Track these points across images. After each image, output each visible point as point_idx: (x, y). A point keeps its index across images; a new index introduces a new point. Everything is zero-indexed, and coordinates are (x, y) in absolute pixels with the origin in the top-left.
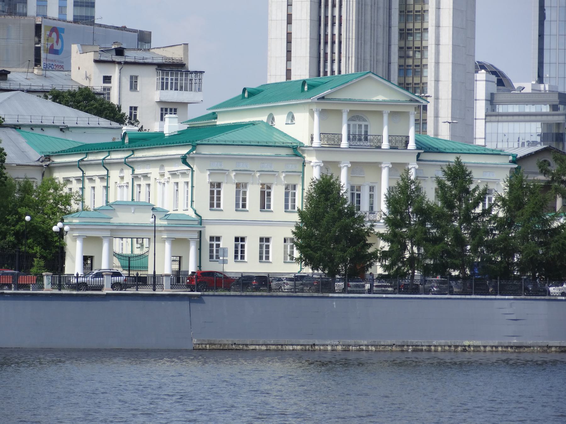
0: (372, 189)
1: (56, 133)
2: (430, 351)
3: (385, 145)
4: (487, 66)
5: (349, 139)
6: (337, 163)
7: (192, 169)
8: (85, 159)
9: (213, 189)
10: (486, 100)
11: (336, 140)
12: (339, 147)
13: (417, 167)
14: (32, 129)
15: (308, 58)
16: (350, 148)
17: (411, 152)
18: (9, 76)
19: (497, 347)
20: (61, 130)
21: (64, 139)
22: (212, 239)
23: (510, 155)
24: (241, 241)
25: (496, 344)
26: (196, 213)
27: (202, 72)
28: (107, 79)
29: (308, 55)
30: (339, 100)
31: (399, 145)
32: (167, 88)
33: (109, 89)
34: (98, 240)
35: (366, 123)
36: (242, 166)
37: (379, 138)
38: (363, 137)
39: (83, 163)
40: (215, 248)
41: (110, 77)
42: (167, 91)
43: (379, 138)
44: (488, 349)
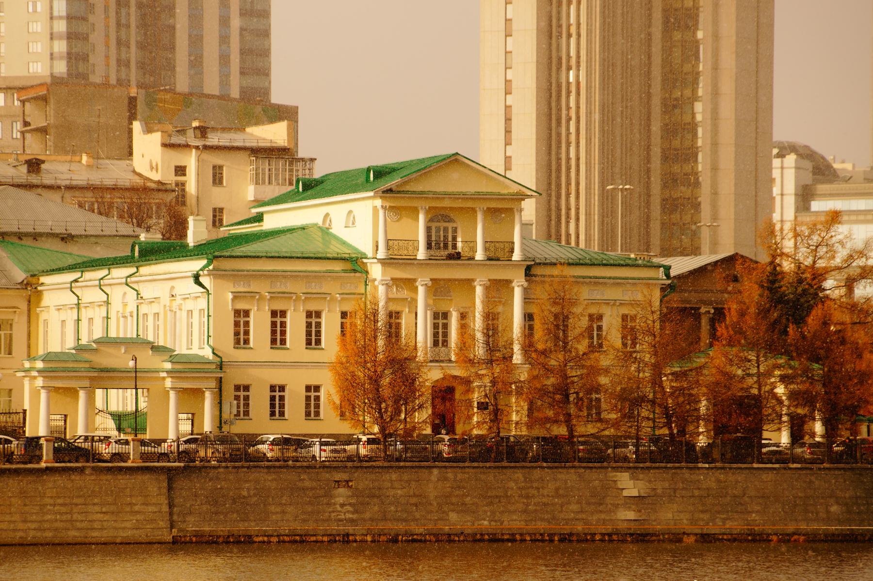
0: (463, 316)
1: (58, 245)
2: (593, 541)
3: (479, 255)
4: (800, 146)
5: (429, 246)
6: (508, 282)
7: (208, 291)
8: (79, 280)
9: (238, 319)
10: (796, 195)
11: (411, 248)
12: (416, 259)
13: (526, 284)
14: (20, 238)
15: (534, 141)
16: (430, 259)
17: (517, 265)
18: (43, 166)
19: (610, 535)
20: (63, 239)
21: (66, 251)
22: (237, 388)
23: (660, 267)
24: (280, 391)
25: (610, 531)
26: (214, 353)
27: (312, 160)
28: (181, 170)
29: (534, 137)
30: (414, 192)
31: (500, 254)
32: (264, 183)
33: (183, 184)
34: (72, 392)
35: (455, 225)
36: (279, 287)
37: (472, 244)
38: (442, 245)
39: (77, 284)
40: (313, 402)
41: (185, 167)
42: (264, 186)
43: (472, 244)
44: (598, 537)
